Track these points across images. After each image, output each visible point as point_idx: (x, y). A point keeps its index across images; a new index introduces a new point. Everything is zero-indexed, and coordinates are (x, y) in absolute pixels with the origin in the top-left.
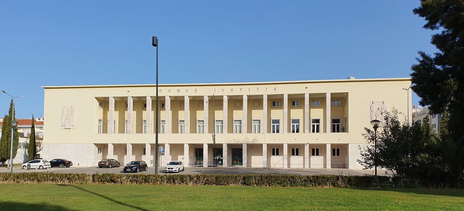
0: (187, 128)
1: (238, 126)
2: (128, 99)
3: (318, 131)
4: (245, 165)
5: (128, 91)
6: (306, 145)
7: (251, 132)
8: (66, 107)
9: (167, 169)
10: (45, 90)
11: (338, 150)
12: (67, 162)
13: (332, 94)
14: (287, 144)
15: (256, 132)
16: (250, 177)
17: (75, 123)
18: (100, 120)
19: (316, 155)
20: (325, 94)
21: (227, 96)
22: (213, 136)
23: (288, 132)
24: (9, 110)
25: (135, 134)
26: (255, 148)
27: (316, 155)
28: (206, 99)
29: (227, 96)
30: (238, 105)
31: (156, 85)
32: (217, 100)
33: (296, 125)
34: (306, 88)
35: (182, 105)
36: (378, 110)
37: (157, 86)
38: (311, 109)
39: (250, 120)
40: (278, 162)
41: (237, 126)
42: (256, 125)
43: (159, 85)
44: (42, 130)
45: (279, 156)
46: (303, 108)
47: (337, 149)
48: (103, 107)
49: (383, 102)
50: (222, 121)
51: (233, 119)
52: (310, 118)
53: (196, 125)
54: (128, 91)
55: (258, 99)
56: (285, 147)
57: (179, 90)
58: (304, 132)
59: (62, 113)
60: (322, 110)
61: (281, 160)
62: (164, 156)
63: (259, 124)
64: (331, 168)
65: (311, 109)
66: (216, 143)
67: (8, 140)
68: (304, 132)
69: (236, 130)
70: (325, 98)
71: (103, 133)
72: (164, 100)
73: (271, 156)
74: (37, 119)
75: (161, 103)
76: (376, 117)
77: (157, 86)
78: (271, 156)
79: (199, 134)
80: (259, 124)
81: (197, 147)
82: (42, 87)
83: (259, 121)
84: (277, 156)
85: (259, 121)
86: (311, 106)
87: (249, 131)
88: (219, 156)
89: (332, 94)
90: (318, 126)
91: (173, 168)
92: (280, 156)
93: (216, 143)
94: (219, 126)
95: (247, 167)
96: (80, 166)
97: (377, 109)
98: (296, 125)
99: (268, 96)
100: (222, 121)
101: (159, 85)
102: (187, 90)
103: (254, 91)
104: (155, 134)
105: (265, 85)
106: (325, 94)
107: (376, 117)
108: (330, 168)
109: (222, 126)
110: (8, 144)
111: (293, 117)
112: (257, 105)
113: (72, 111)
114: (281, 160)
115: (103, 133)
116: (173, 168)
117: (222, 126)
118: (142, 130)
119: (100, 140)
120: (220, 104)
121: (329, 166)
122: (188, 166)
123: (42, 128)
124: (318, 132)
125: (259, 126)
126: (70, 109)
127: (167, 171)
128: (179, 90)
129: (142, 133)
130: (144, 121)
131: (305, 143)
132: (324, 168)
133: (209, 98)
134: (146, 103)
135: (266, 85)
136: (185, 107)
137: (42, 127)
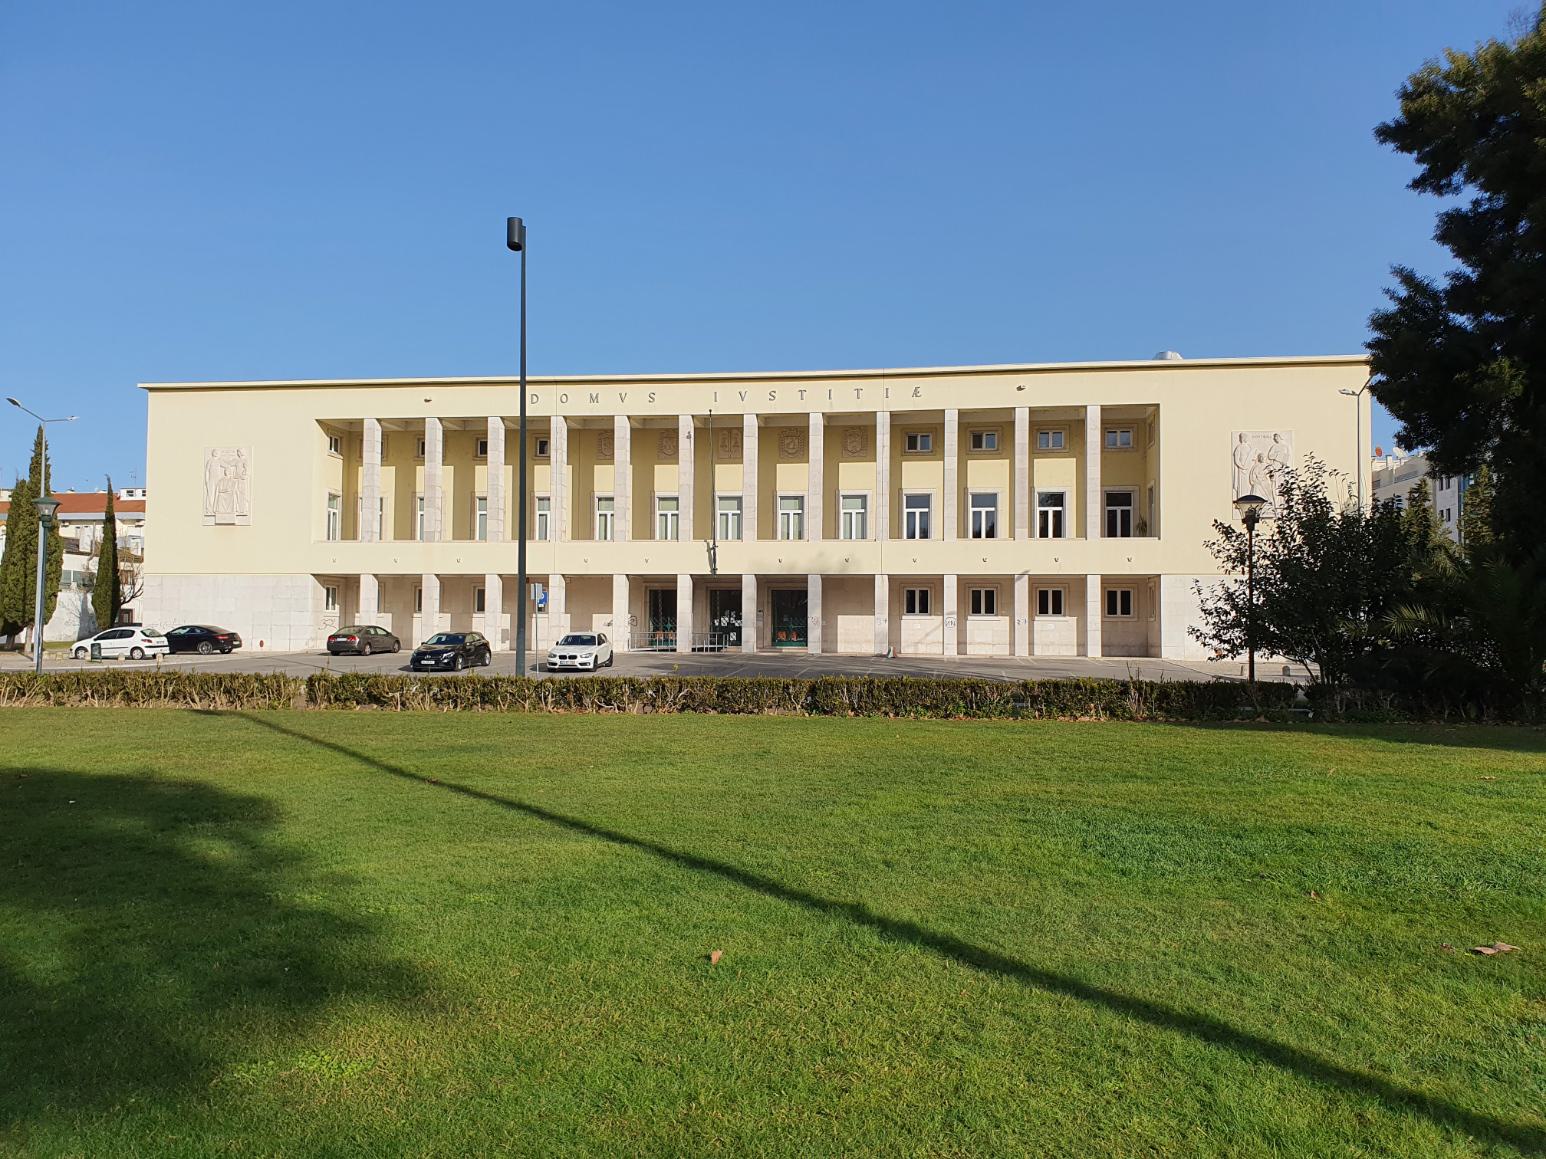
2: (427, 425)
4: (814, 646)
5: (427, 401)
6: (1019, 579)
8: (219, 454)
10: (151, 395)
11: (1126, 596)
12: (223, 635)
13: (1104, 409)
16: (833, 686)
18: (332, 497)
19: (1053, 613)
22: (709, 550)
23: (958, 537)
25: (449, 542)
26: (850, 591)
27: (1053, 613)
28: (686, 427)
29: (757, 415)
30: (791, 446)
31: (518, 378)
34: (1020, 389)
37: (523, 383)
40: (927, 635)
41: (788, 514)
43: (528, 378)
44: (138, 528)
45: (929, 617)
46: (1010, 453)
50: (739, 499)
51: (774, 491)
56: (948, 587)
57: (597, 397)
58: (1012, 535)
59: (208, 473)
60: (1071, 463)
61: (935, 629)
62: (546, 615)
64: (1103, 656)
66: (718, 572)
68: (1012, 535)
70: (1082, 423)
71: (342, 539)
73: (904, 617)
75: (537, 439)
76: (1253, 486)
77: (523, 383)
78: (904, 617)
79: (664, 543)
80: (863, 511)
82: (140, 385)
83: (864, 498)
84: (924, 617)
86: (1036, 450)
87: (831, 531)
88: (730, 616)
89: (1104, 409)
90: (1058, 516)
91: (574, 657)
93: (718, 572)
94: (730, 515)
96: (265, 648)
97: (1256, 458)
100: (739, 499)
101: (528, 378)
102: (623, 395)
103: (846, 398)
104: (516, 544)
105: (553, 387)
107: (1253, 486)
108: (1100, 655)
109: (738, 515)
110: (26, 577)
111: (976, 486)
113: (240, 465)
114: (935, 629)
115: (342, 539)
116: (574, 657)
117: (739, 517)
121: (1095, 650)
122: (626, 649)
123: (141, 523)
124: (1060, 536)
125: (863, 515)
127: (557, 667)
128: (597, 397)
131: (1016, 571)
132: (1078, 656)
134: (487, 438)
135: (887, 380)
137: (139, 521)
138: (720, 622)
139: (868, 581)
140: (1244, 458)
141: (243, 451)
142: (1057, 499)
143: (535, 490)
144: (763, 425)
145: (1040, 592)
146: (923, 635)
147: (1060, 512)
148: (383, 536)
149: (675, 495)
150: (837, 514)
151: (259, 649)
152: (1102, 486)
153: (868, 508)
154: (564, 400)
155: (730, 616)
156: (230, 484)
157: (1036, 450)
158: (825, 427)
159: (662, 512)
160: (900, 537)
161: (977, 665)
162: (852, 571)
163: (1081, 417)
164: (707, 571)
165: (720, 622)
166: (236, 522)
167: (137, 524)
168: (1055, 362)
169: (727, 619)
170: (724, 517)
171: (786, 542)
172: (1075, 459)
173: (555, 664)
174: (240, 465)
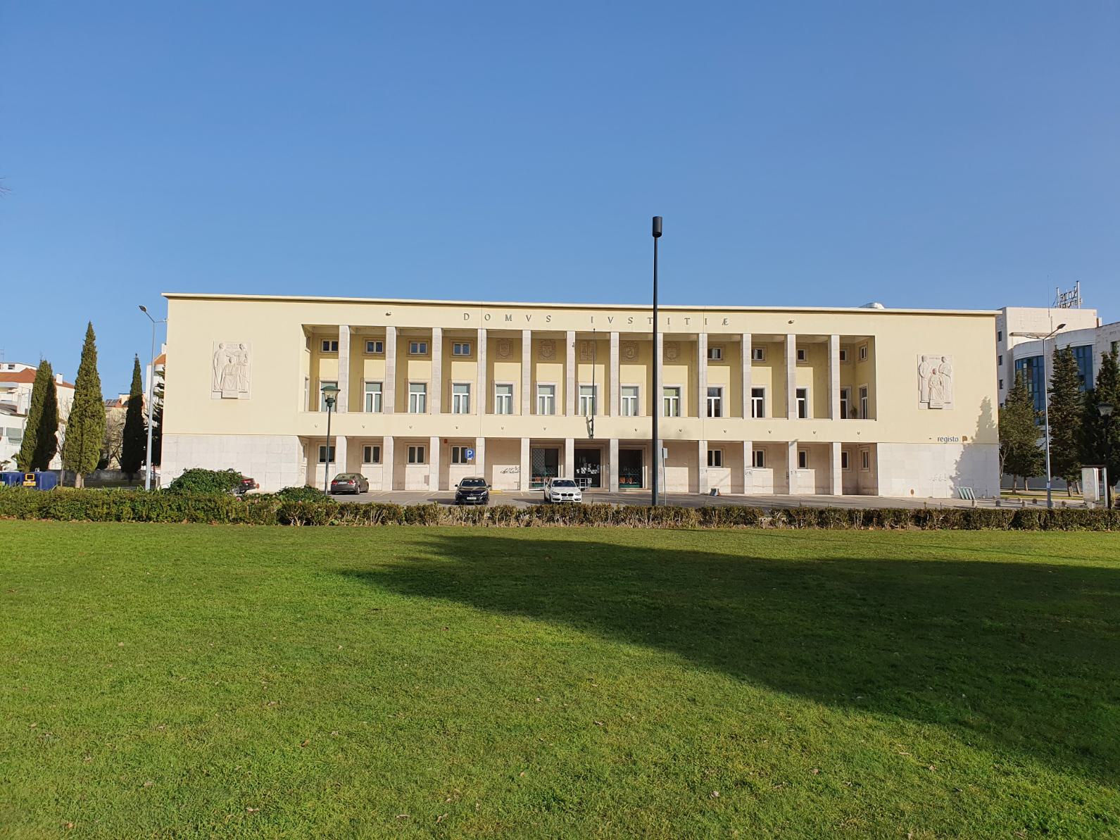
0: (434, 401)
1: (630, 400)
2: (387, 332)
3: (718, 414)
4: (646, 488)
5: (387, 314)
6: (792, 445)
7: (406, 411)
8: (224, 347)
9: (560, 497)
10: (170, 301)
11: (717, 453)
12: (246, 480)
13: (753, 336)
14: (438, 439)
15: (671, 415)
16: (1031, 513)
17: (249, 386)
18: (306, 379)
19: (758, 466)
20: (608, 334)
21: (396, 327)
22: (588, 422)
23: (531, 413)
24: (82, 350)
25: (770, 419)
26: (683, 451)
27: (758, 466)
28: (571, 339)
29: (396, 327)
30: (630, 353)
31: (652, 307)
32: (585, 340)
33: (758, 401)
34: (790, 322)
35: (502, 349)
36: (934, 373)
37: (655, 310)
38: (538, 365)
39: (403, 383)
40: (721, 480)
41: (459, 396)
42: (372, 395)
43: (659, 307)
44: (11, 395)
45: (423, 466)
46: (564, 361)
47: (419, 448)
48: (311, 347)
49: (943, 358)
50: (510, 386)
51: (406, 379)
52: (576, 382)
53: (406, 393)
54: (387, 314)
55: (675, 342)
56: (746, 449)
57: (510, 317)
58: (565, 413)
59: (216, 360)
60: (520, 364)
61: (726, 477)
62: (381, 465)
63: (467, 394)
64: (843, 494)
65: (538, 365)
66: (594, 437)
67: (82, 425)
68: (565, 413)
69: (457, 405)
70: (608, 341)
71: (309, 411)
72: (337, 332)
73: (451, 466)
74: (7, 365)
75: (410, 342)
76: (930, 389)
77: (655, 310)
78: (363, 465)
79: (543, 417)
80: (467, 394)
81: (538, 445)
82: (163, 294)
83: (468, 385)
84: (420, 465)
85: (468, 385)
86: (579, 359)
87: (446, 408)
88: (588, 467)
89: (753, 336)
90: (718, 403)
91: (572, 495)
92: (724, 469)
93: (594, 437)
94: (546, 398)
95: (816, 494)
96: (916, 495)
97: (932, 371)
98: (758, 401)
99: (533, 333)
100: (510, 386)
101: (659, 307)
102: (529, 317)
103: (455, 319)
104: (651, 418)
105: (702, 313)
106: (608, 334)
107: (930, 389)
108: (841, 494)
109: (467, 396)
110: (82, 436)
111: (368, 376)
112: (672, 355)
113: (243, 355)
114: (726, 477)
115: (309, 411)
116: (572, 495)
117: (510, 399)
118: (449, 406)
119: (545, 429)
120: (591, 349)
121: (838, 491)
122: (525, 488)
123: (13, 391)
124: (719, 416)
125: (468, 397)
126: (235, 350)
127: (560, 501)
128: (510, 317)
129: (407, 412)
130: (411, 384)
131: (790, 440)
132: (816, 494)
133: (352, 331)
134: (338, 339)
135: (706, 313)
136: (523, 354)
137: (11, 389)
138: (580, 471)
139: (517, 442)
140: (925, 371)
141: (245, 345)
142: (719, 392)
143: (452, 378)
144: (354, 333)
145: (366, 448)
146: (718, 480)
147: (719, 400)
148: (428, 408)
149: (381, 381)
150: (492, 395)
151: (910, 496)
152: (841, 386)
153: (471, 393)
154: (466, 316)
155: (588, 467)
156: (234, 369)
157: (625, 358)
158: (443, 337)
159: (541, 395)
160: (449, 411)
161: (810, 501)
162: (685, 438)
163: (608, 338)
164: (587, 437)
165: (580, 471)
166: (239, 397)
167: (9, 391)
168: (479, 301)
169: (585, 469)
170: (499, 398)
171: (500, 416)
172: (812, 368)
173: (559, 500)
174: (243, 355)
